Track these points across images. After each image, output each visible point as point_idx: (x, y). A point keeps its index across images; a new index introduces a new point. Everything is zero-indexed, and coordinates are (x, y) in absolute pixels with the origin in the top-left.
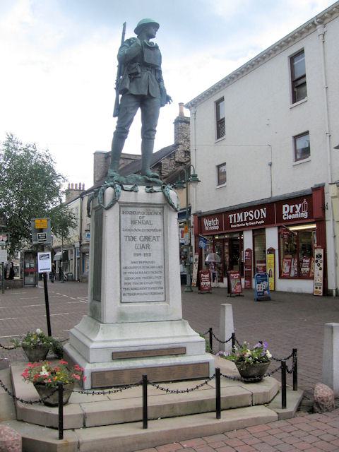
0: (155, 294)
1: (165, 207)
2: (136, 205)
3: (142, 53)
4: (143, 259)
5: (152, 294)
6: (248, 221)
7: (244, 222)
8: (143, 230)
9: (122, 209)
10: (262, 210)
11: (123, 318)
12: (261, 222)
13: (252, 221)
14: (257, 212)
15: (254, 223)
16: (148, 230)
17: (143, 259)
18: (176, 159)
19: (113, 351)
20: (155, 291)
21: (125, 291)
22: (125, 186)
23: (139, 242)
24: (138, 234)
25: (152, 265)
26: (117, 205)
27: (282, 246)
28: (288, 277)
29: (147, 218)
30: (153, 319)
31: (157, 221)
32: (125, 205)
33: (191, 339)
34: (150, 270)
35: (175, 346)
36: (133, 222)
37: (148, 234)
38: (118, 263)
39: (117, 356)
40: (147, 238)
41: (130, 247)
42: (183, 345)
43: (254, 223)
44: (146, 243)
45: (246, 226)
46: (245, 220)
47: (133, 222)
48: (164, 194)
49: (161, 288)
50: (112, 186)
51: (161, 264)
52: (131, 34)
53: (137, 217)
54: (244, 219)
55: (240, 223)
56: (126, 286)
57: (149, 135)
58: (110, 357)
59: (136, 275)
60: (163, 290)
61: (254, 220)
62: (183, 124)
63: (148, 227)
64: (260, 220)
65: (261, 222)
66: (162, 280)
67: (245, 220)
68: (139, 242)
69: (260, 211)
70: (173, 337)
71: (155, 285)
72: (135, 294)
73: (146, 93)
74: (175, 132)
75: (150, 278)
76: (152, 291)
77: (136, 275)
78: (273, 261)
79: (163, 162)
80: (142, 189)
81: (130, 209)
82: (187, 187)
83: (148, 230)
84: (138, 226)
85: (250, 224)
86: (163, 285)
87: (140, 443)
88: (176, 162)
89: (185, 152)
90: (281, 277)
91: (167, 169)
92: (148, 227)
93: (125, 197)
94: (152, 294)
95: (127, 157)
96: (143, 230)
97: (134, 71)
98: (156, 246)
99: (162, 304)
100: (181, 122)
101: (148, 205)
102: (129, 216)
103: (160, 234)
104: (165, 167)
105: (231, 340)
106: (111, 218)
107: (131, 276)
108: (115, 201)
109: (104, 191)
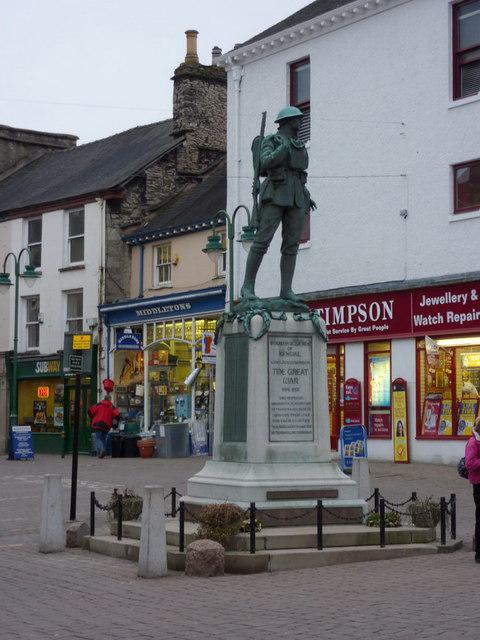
0: (303, 432)
1: (314, 338)
2: (283, 334)
3: (288, 156)
4: (291, 394)
5: (299, 433)
6: (356, 324)
7: (347, 326)
8: (292, 363)
9: (271, 339)
10: (385, 304)
11: (271, 457)
12: (382, 328)
13: (363, 325)
14: (375, 306)
15: (368, 329)
16: (297, 363)
17: (291, 394)
18: (180, 167)
19: (141, 549)
20: (304, 430)
21: (273, 429)
22: (273, 313)
23: (286, 375)
24: (286, 367)
25: (300, 401)
26: (266, 336)
27: (422, 375)
28: (434, 436)
29: (295, 349)
30: (302, 459)
31: (304, 351)
32: (276, 334)
33: (343, 482)
34: (298, 407)
35: (327, 488)
36: (282, 354)
37: (297, 367)
38: (266, 398)
39: (273, 496)
40: (296, 372)
41: (278, 382)
42: (335, 488)
43: (368, 329)
44: (294, 377)
45: (350, 335)
46: (350, 321)
47: (282, 354)
48: (313, 323)
49: (309, 426)
50: (260, 314)
51: (309, 400)
52: (272, 129)
53: (285, 348)
54: (346, 319)
55: (338, 327)
56: (275, 424)
57: (292, 251)
58: (264, 497)
59: (284, 412)
60: (311, 429)
61: (369, 323)
62: (196, 82)
63: (296, 359)
64: (380, 323)
65: (382, 328)
66: (310, 418)
67: (350, 321)
68: (286, 375)
69: (382, 306)
70: (324, 479)
71: (303, 423)
72: (283, 433)
73: (292, 204)
74: (176, 101)
75: (299, 415)
76: (302, 429)
77: (284, 412)
78: (404, 405)
79: (149, 173)
80: (290, 316)
81: (278, 340)
82: (390, 351)
83: (297, 363)
84: (287, 358)
85: (360, 329)
86: (311, 424)
87: (319, 554)
88: (180, 174)
89: (201, 150)
90: (419, 436)
91: (158, 189)
92: (296, 359)
93: (275, 326)
94: (299, 433)
95: (32, 139)
96: (292, 363)
97: (280, 178)
98: (304, 380)
99: (310, 444)
100: (192, 77)
101: (297, 335)
102: (277, 347)
103: (308, 367)
104: (154, 184)
105: (373, 498)
106: (257, 353)
107: (279, 412)
108: (265, 331)
109: (250, 319)
